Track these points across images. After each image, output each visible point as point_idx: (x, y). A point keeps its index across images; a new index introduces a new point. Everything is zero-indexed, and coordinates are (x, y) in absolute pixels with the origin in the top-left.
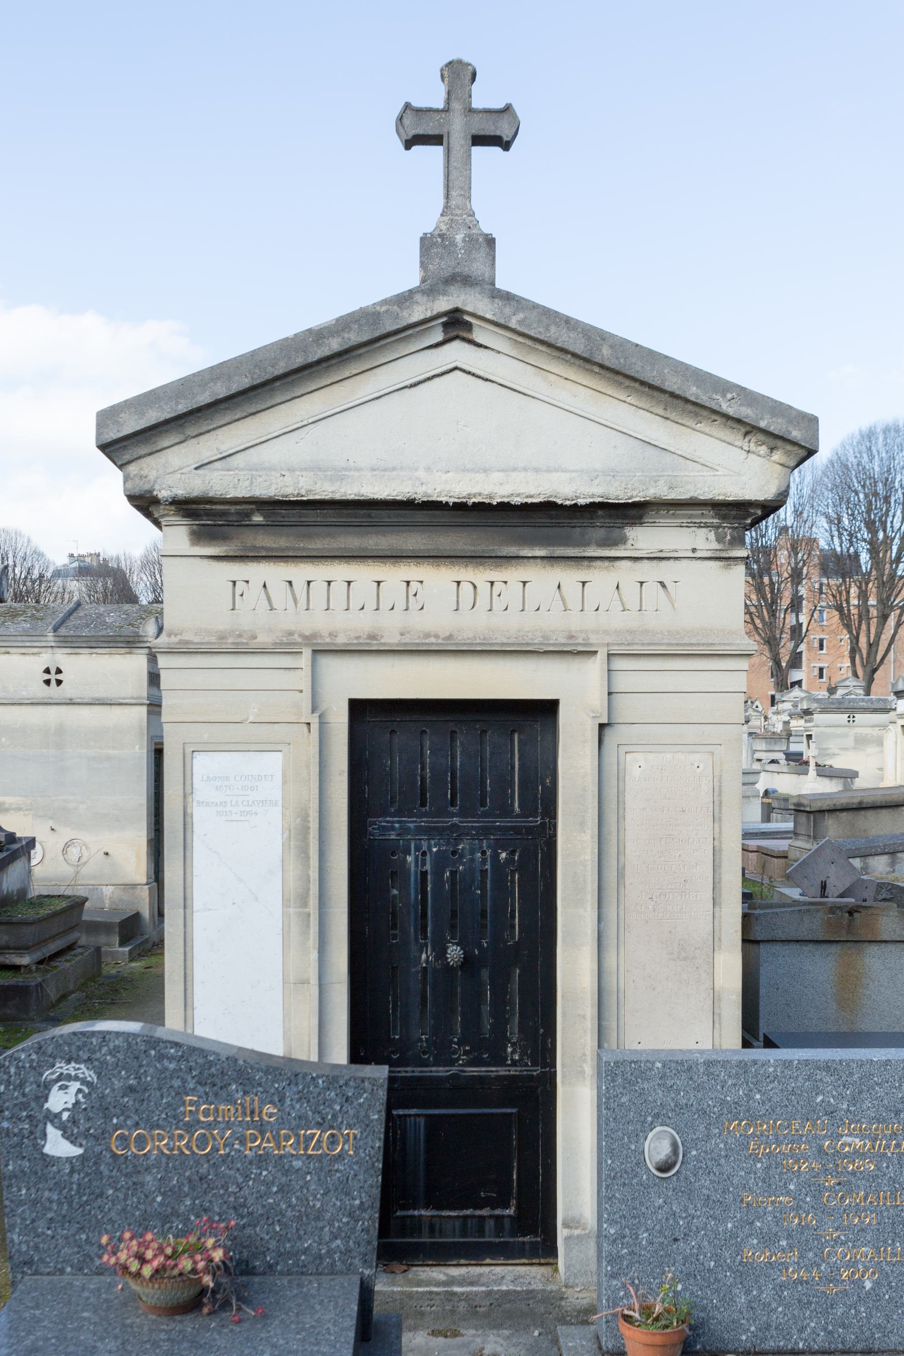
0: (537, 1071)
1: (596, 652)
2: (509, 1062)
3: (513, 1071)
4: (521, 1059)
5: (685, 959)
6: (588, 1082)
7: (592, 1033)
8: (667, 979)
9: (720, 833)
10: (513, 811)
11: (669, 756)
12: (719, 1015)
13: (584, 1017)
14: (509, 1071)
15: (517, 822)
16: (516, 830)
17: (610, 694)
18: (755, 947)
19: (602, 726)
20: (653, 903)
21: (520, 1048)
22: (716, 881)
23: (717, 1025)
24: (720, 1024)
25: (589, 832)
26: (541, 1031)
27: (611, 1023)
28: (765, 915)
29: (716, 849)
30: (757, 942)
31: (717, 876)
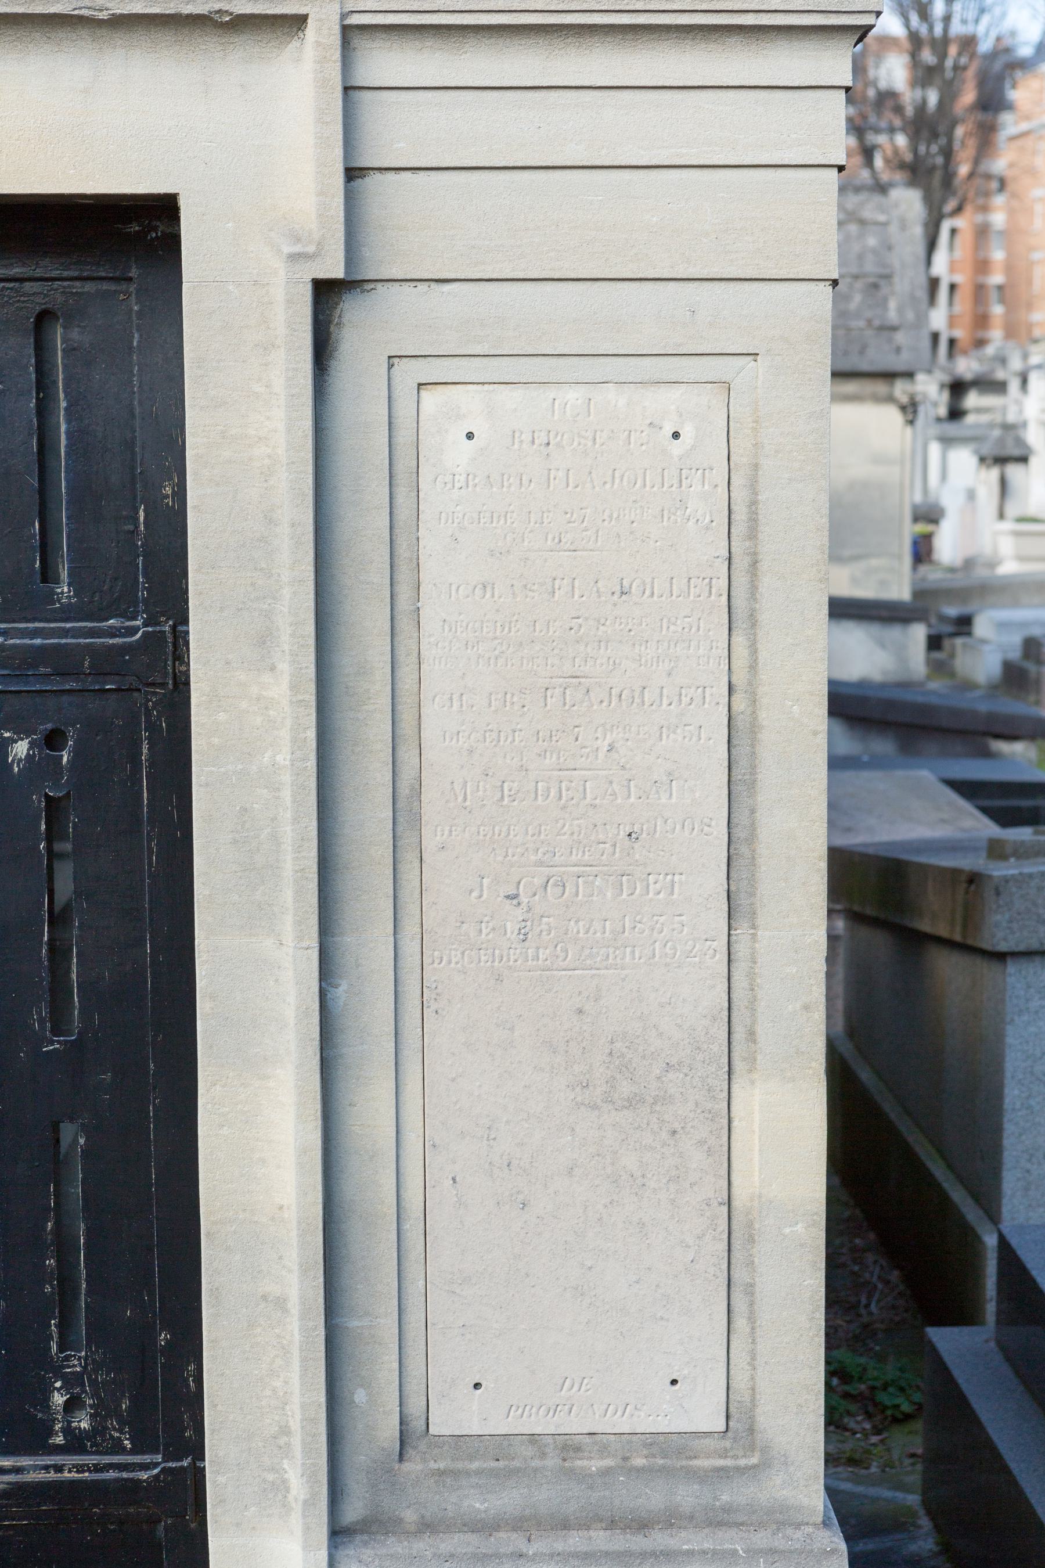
0: (149, 1467)
1: (299, 21)
2: (59, 1440)
3: (71, 1469)
4: (98, 1430)
5: (630, 1103)
6: (296, 1520)
7: (304, 1360)
8: (570, 1171)
9: (753, 667)
10: (50, 597)
11: (573, 396)
12: (750, 1289)
13: (281, 1303)
14: (59, 1469)
15: (65, 633)
16: (64, 664)
17: (353, 173)
18: (987, 970)
19: (326, 293)
20: (519, 913)
21: (95, 1395)
22: (739, 833)
23: (741, 1323)
24: (752, 1319)
25: (284, 667)
26: (163, 1337)
27: (375, 1320)
28: (1023, 879)
29: (740, 722)
30: (1001, 957)
31: (742, 818)
